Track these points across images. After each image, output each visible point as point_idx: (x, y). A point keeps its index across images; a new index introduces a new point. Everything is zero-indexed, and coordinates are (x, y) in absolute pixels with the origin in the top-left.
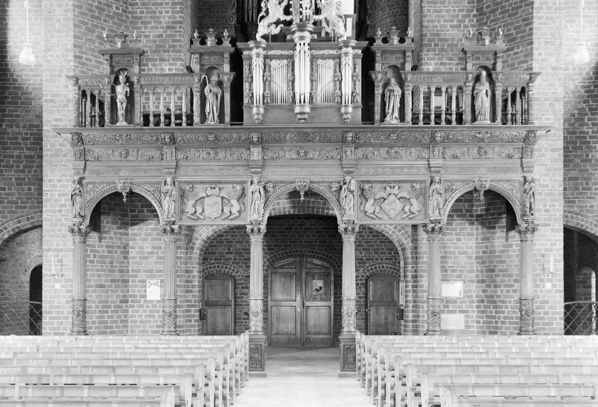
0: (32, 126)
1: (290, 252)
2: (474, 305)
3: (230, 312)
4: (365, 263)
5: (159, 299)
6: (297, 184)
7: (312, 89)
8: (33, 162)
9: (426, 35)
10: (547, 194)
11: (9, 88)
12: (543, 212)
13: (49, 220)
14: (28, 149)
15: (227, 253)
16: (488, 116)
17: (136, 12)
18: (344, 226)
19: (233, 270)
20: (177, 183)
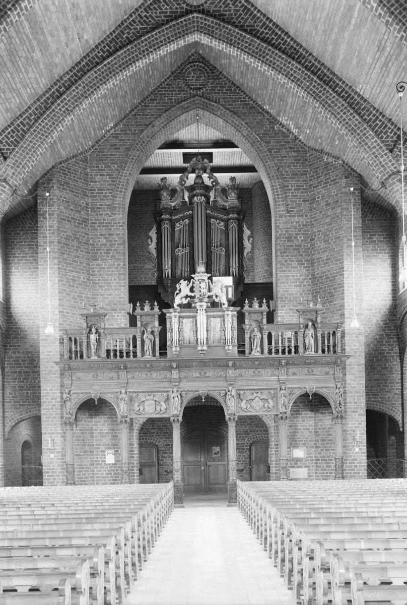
0: (28, 352)
1: (196, 427)
2: (314, 462)
3: (155, 469)
4: (249, 434)
5: (114, 462)
6: (200, 392)
7: (207, 335)
8: (29, 375)
9: (280, 292)
10: (355, 393)
11: (12, 328)
12: (353, 404)
13: (46, 414)
14: (26, 367)
15: (151, 429)
16: (313, 350)
17: (95, 280)
18: (229, 417)
19: (156, 441)
20: (128, 393)
